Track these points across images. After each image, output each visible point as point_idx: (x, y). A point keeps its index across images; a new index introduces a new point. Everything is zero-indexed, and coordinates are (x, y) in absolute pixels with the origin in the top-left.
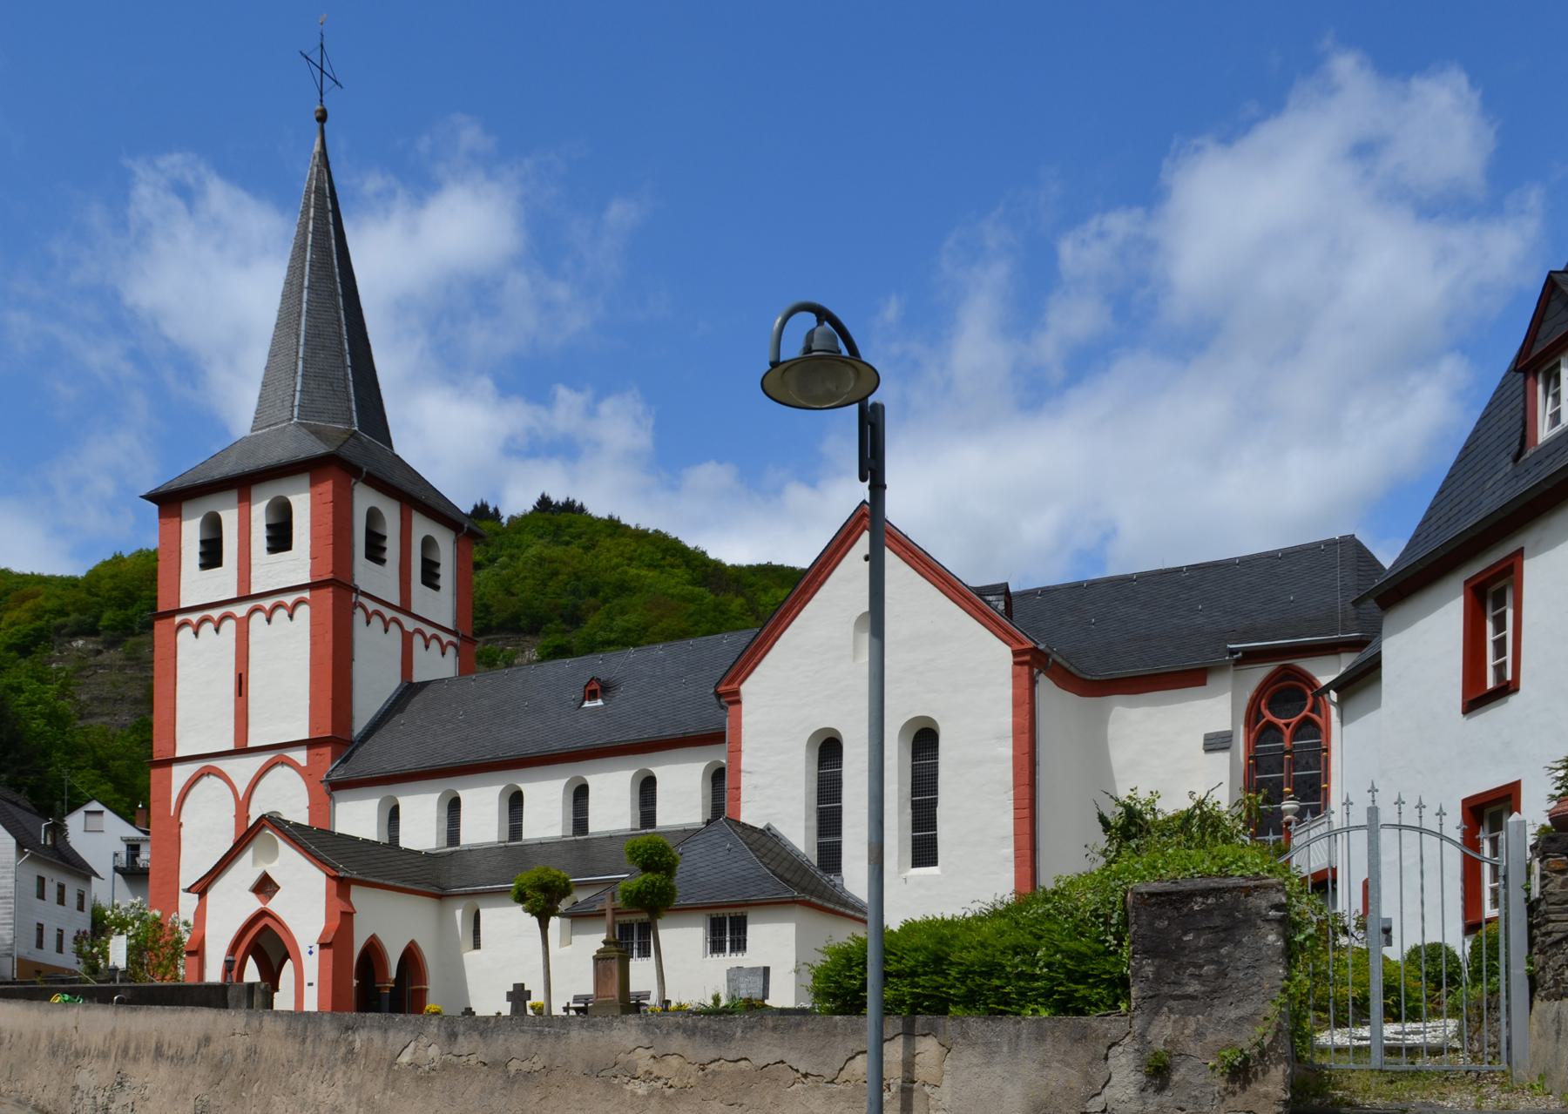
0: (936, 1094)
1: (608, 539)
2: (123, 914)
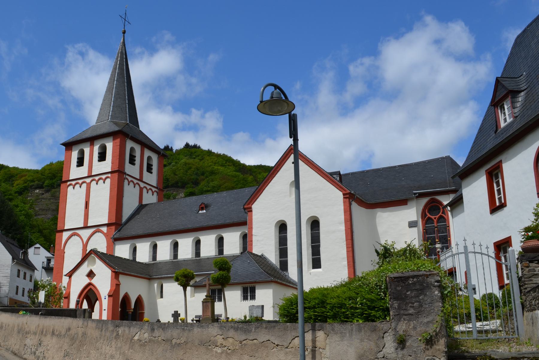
1: (208, 157)
2: (44, 283)
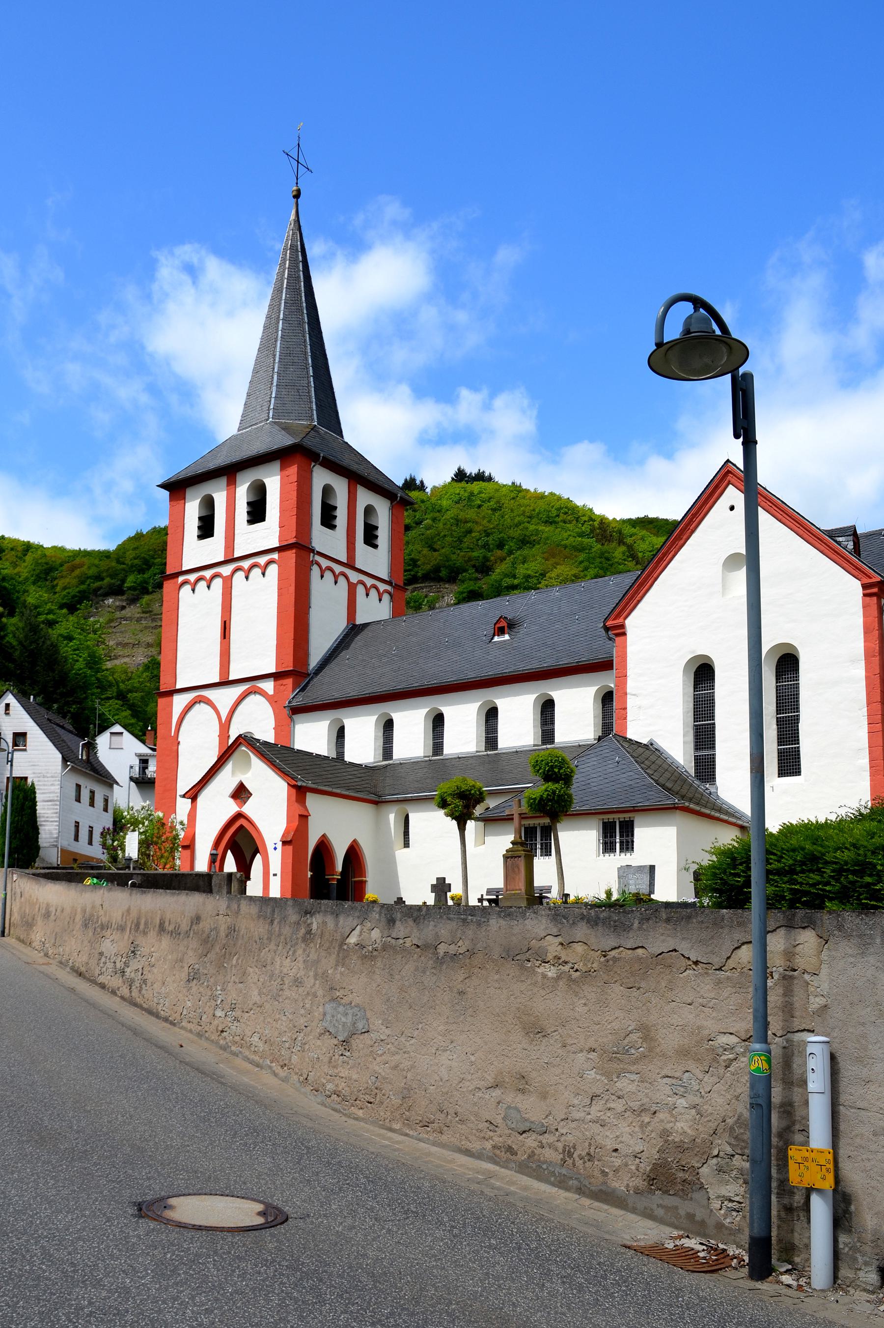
0: (815, 981)
